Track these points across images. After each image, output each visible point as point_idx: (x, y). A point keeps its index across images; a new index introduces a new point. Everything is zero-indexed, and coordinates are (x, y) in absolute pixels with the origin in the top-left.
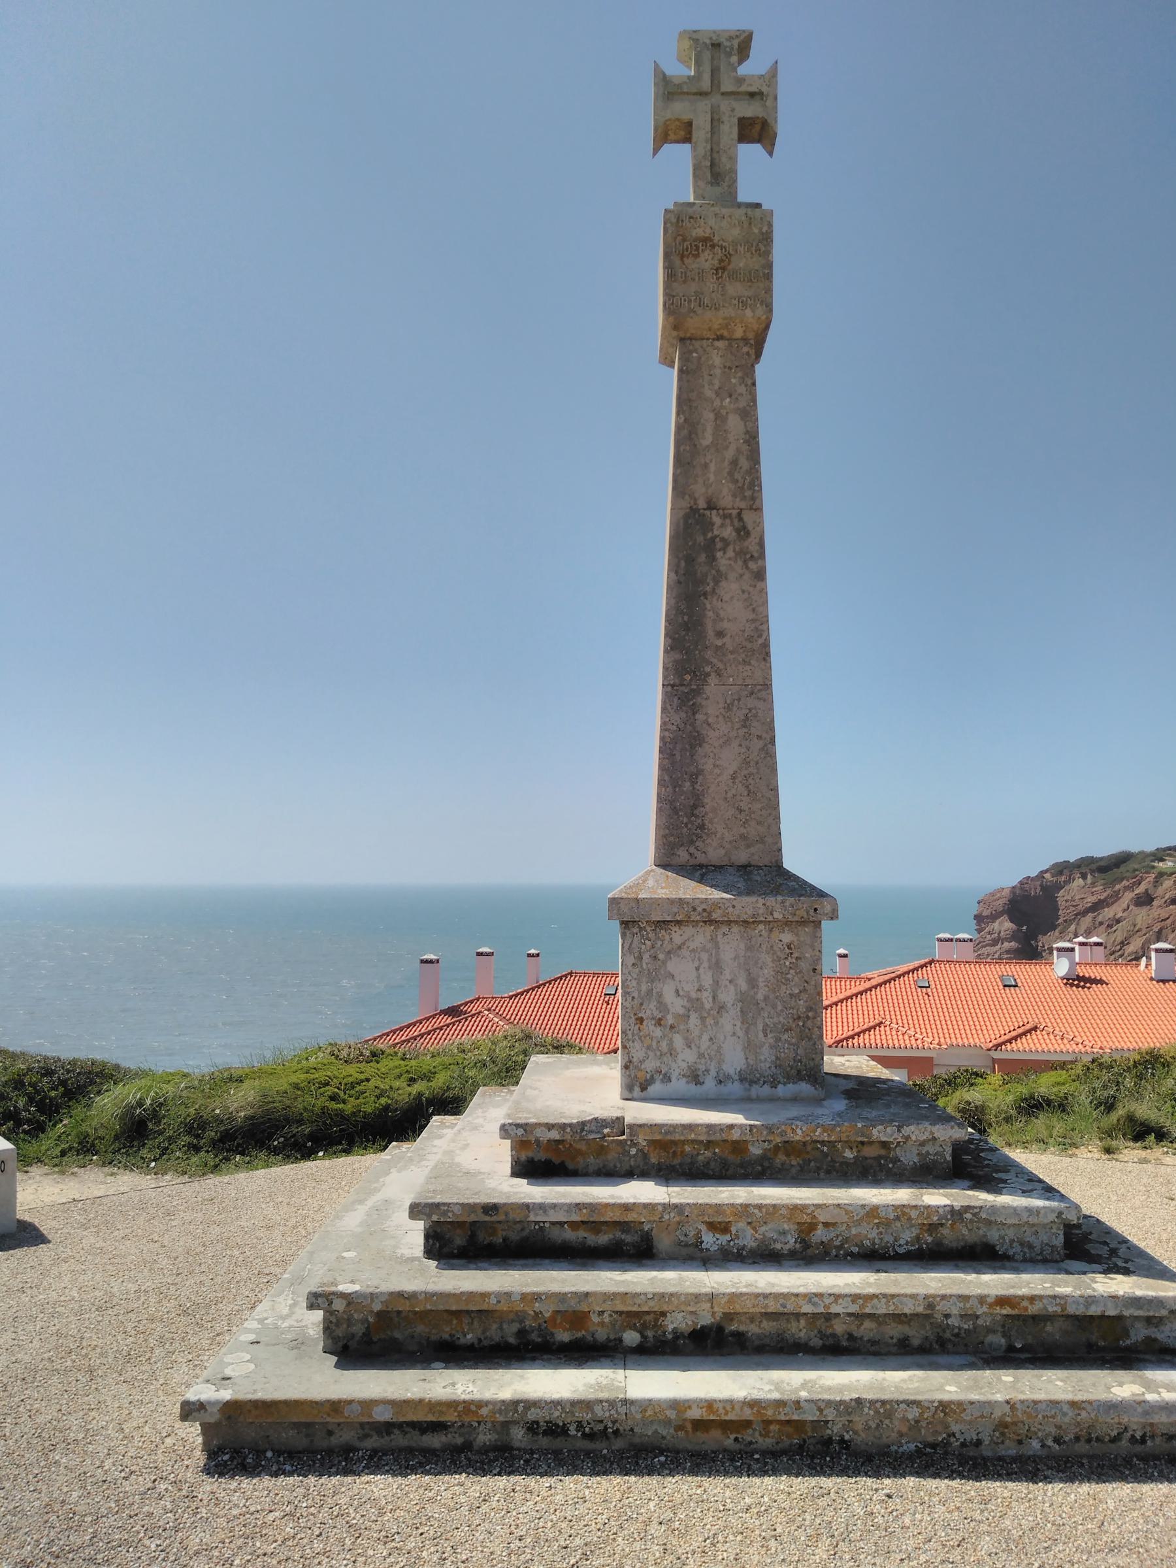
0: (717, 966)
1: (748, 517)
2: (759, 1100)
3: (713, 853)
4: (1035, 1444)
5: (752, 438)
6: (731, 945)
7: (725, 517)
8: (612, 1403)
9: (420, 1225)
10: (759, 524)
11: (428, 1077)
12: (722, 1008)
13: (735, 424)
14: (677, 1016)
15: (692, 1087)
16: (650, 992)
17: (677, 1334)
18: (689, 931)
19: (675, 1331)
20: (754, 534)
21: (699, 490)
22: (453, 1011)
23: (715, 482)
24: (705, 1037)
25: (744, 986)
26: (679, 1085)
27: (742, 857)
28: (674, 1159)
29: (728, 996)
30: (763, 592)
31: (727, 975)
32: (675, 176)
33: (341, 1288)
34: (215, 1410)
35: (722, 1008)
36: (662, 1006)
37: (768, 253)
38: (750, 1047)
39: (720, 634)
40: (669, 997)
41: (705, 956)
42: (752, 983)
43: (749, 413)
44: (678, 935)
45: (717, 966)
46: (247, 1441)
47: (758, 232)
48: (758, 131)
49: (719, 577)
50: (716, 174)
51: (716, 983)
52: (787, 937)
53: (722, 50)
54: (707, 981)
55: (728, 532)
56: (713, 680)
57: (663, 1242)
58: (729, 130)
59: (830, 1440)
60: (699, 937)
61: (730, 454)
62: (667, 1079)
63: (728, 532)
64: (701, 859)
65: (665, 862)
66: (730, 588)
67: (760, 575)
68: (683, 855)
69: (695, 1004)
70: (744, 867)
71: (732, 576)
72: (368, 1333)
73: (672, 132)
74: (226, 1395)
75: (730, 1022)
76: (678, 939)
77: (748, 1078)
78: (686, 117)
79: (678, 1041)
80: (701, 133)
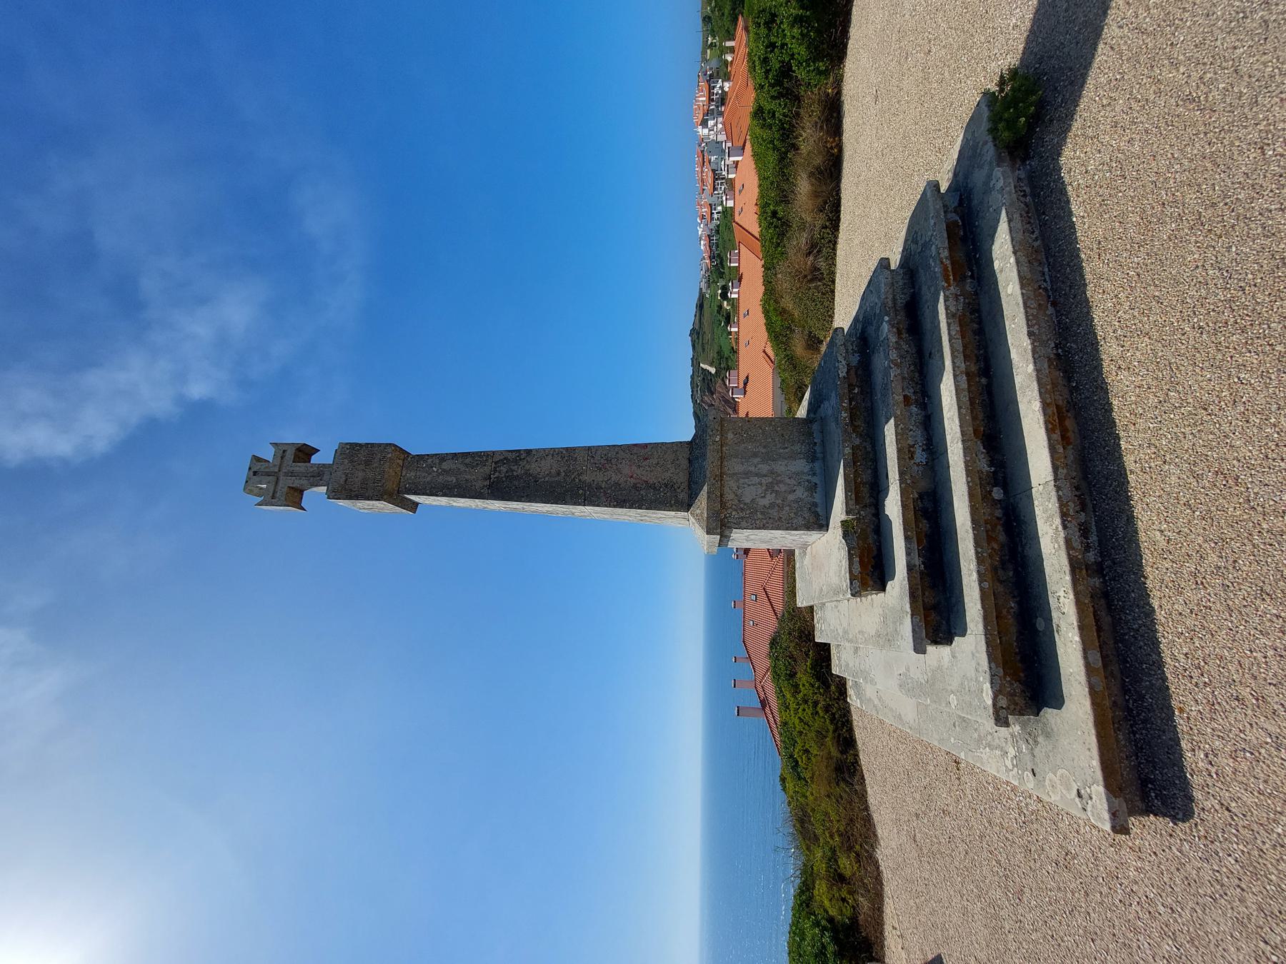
0: (747, 474)
1: (497, 458)
2: (824, 452)
3: (682, 478)
4: (1036, 244)
5: (455, 456)
6: (735, 466)
7: (495, 471)
8: (1058, 488)
9: (931, 649)
10: (501, 452)
11: (946, 269)
12: (772, 472)
13: (445, 466)
14: (776, 498)
15: (819, 489)
16: (762, 513)
17: (991, 464)
18: (726, 489)
19: (990, 466)
20: (506, 455)
21: (479, 484)
22: (764, 707)
23: (476, 476)
24: (788, 481)
25: (756, 460)
26: (818, 498)
27: (685, 463)
28: (868, 493)
29: (764, 468)
30: (537, 450)
31: (752, 469)
32: (316, 495)
33: (990, 702)
34: (1116, 801)
35: (772, 472)
36: (772, 505)
37: (360, 445)
38: (792, 457)
39: (559, 474)
40: (766, 502)
41: (741, 481)
42: (755, 455)
43: (442, 458)
44: (729, 496)
45: (747, 474)
46: (1146, 772)
47: (350, 452)
48: (304, 452)
49: (527, 473)
50: (318, 476)
51: (757, 475)
52: (730, 436)
53: (258, 469)
54: (756, 480)
55: (504, 469)
56: (584, 478)
57: (924, 485)
58: (301, 467)
59: (1058, 355)
60: (730, 483)
61: (463, 468)
62: (815, 505)
63: (504, 469)
64: (685, 485)
65: (686, 506)
66: (534, 467)
67: (529, 452)
68: (683, 496)
69: (770, 487)
70: (690, 461)
71: (528, 467)
72: (1026, 682)
73: (294, 498)
74: (1099, 790)
75: (780, 467)
76: (731, 496)
77: (812, 458)
78: (285, 489)
79: (791, 497)
80: (297, 483)
